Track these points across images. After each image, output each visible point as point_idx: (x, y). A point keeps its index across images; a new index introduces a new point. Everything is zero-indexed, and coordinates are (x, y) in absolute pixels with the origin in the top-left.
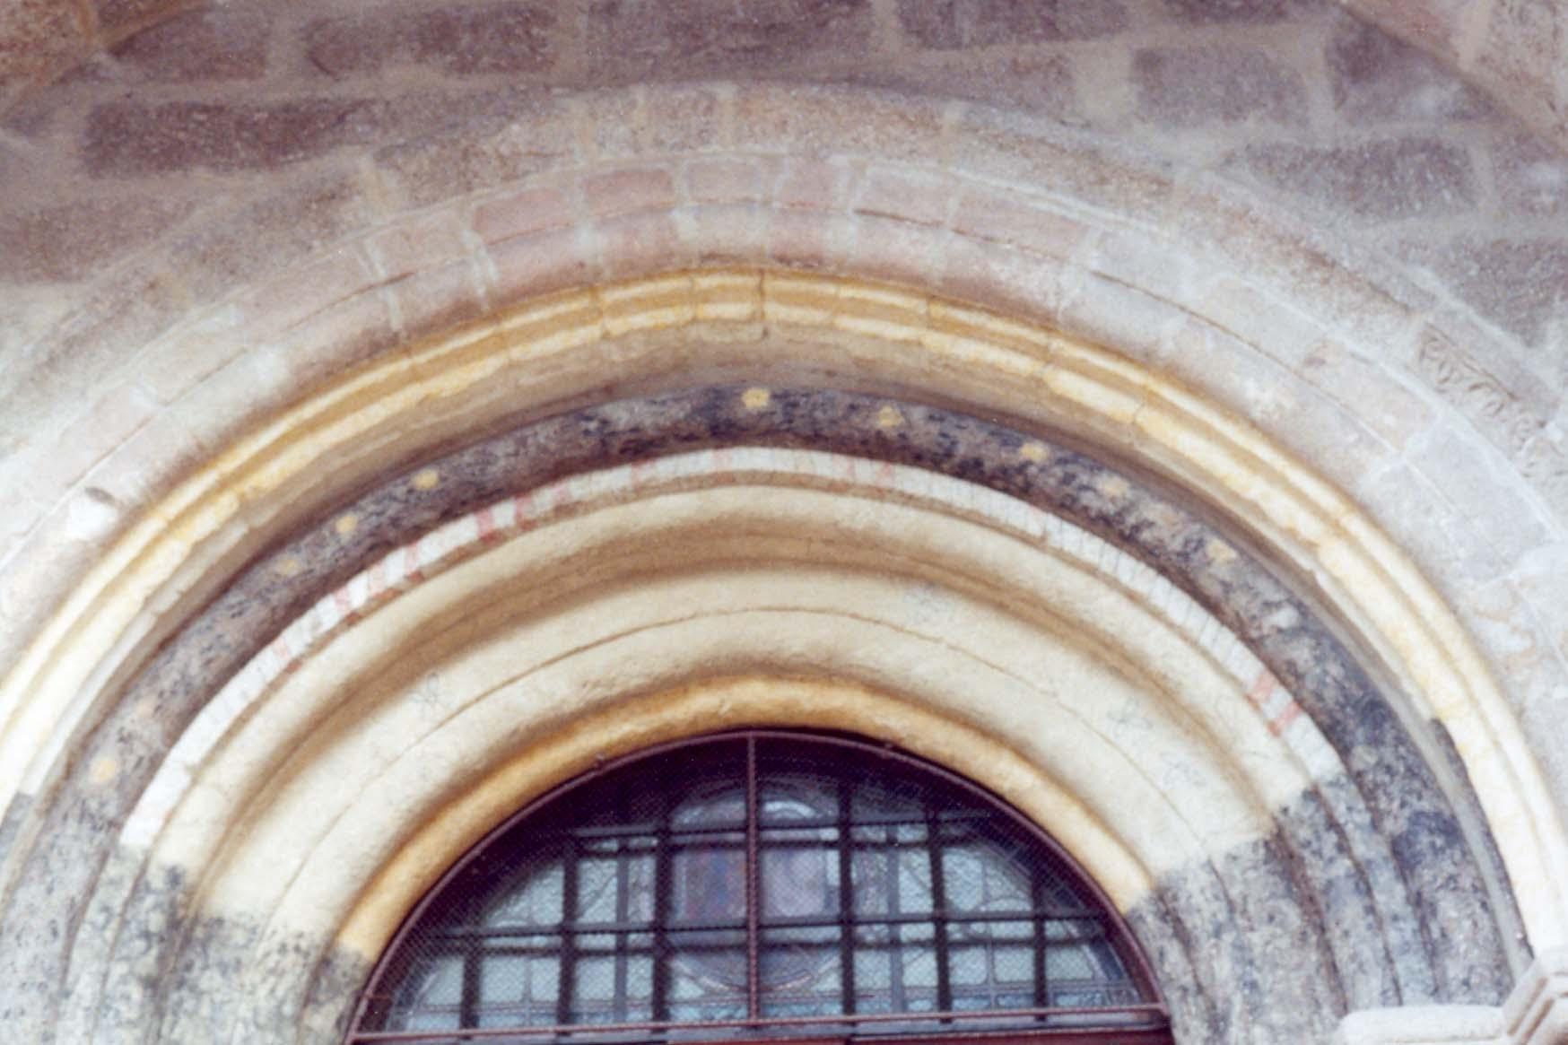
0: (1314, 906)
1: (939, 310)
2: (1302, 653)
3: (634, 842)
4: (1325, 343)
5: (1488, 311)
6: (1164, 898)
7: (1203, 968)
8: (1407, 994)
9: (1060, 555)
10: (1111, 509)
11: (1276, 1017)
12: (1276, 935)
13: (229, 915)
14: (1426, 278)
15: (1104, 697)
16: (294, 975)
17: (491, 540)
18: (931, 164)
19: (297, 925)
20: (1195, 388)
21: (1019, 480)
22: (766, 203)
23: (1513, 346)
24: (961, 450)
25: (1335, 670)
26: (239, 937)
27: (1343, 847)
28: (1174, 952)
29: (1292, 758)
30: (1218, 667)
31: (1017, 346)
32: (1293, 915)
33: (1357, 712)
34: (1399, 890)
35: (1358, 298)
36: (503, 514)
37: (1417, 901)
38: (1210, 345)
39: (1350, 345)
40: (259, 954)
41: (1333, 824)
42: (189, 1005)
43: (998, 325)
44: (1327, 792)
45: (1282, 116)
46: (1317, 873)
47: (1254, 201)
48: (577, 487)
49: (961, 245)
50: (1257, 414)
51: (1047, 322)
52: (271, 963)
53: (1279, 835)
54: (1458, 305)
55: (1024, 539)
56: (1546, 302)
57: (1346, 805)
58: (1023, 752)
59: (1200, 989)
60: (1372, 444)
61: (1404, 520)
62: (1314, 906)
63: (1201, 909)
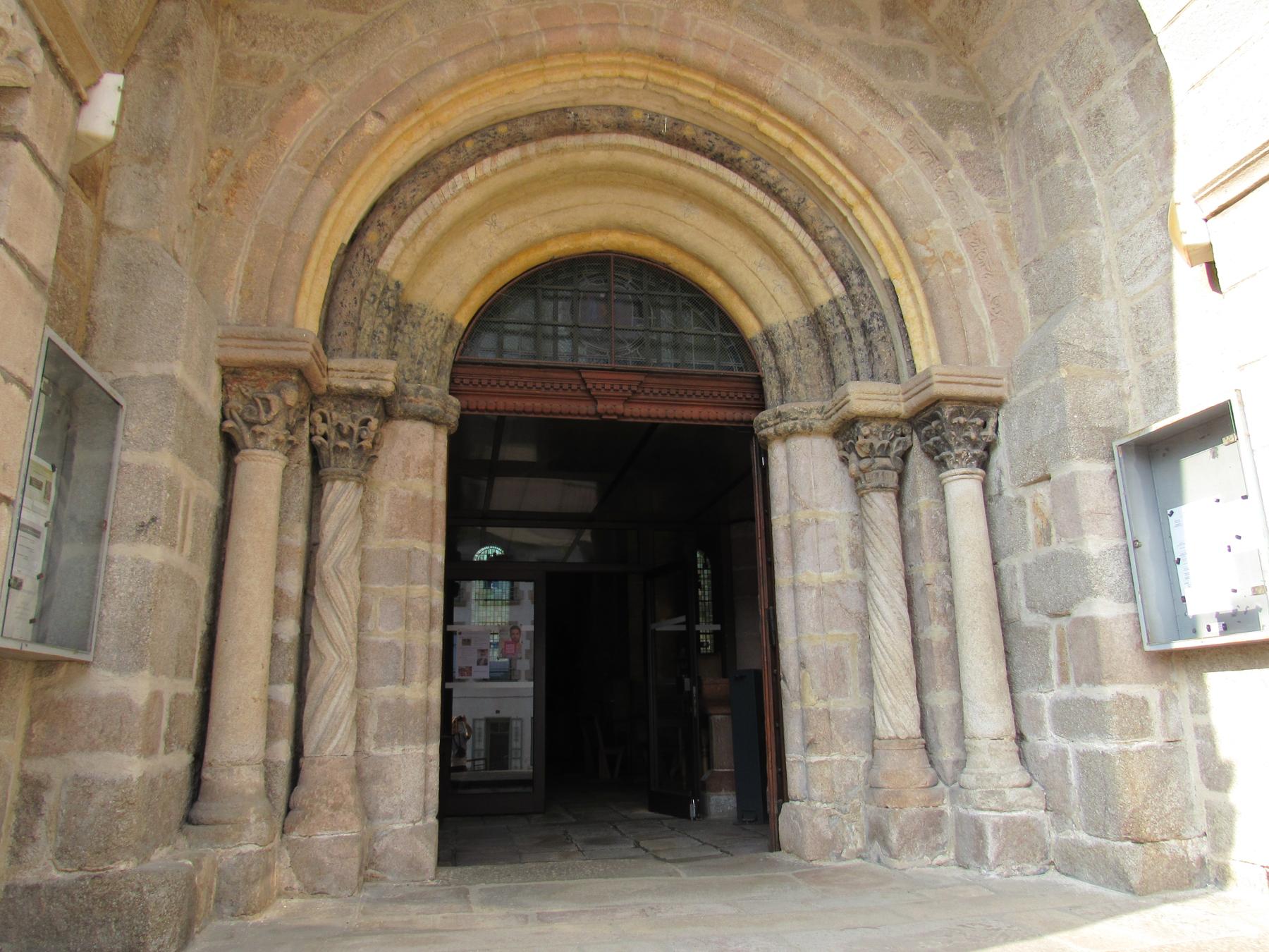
0: (826, 346)
1: (721, 88)
2: (838, 248)
3: (560, 293)
4: (869, 126)
5: (931, 123)
6: (768, 335)
7: (781, 361)
8: (861, 377)
9: (748, 197)
10: (772, 181)
11: (808, 381)
12: (810, 351)
13: (415, 303)
14: (910, 105)
15: (755, 256)
16: (440, 332)
17: (525, 159)
18: (724, 23)
19: (442, 310)
20: (818, 137)
21: (737, 165)
22: (657, 30)
23: (939, 138)
24: (716, 149)
25: (849, 256)
26: (419, 313)
27: (843, 321)
28: (768, 355)
29: (828, 288)
30: (804, 249)
31: (749, 108)
32: (815, 345)
33: (850, 271)
34: (862, 340)
35: (884, 110)
36: (531, 148)
37: (869, 344)
38: (827, 120)
39: (878, 129)
40: (426, 320)
41: (839, 313)
42: (400, 338)
43: (743, 98)
44: (840, 302)
45: (862, 29)
46: (831, 330)
47: (851, 63)
48: (560, 141)
49: (735, 61)
50: (841, 150)
51: (763, 99)
52: (432, 324)
53: (817, 314)
54: (921, 119)
55: (734, 188)
56: (951, 123)
57: (846, 307)
58: (719, 273)
59: (778, 369)
60: (883, 170)
61: (890, 200)
62: (826, 346)
63: (782, 339)
